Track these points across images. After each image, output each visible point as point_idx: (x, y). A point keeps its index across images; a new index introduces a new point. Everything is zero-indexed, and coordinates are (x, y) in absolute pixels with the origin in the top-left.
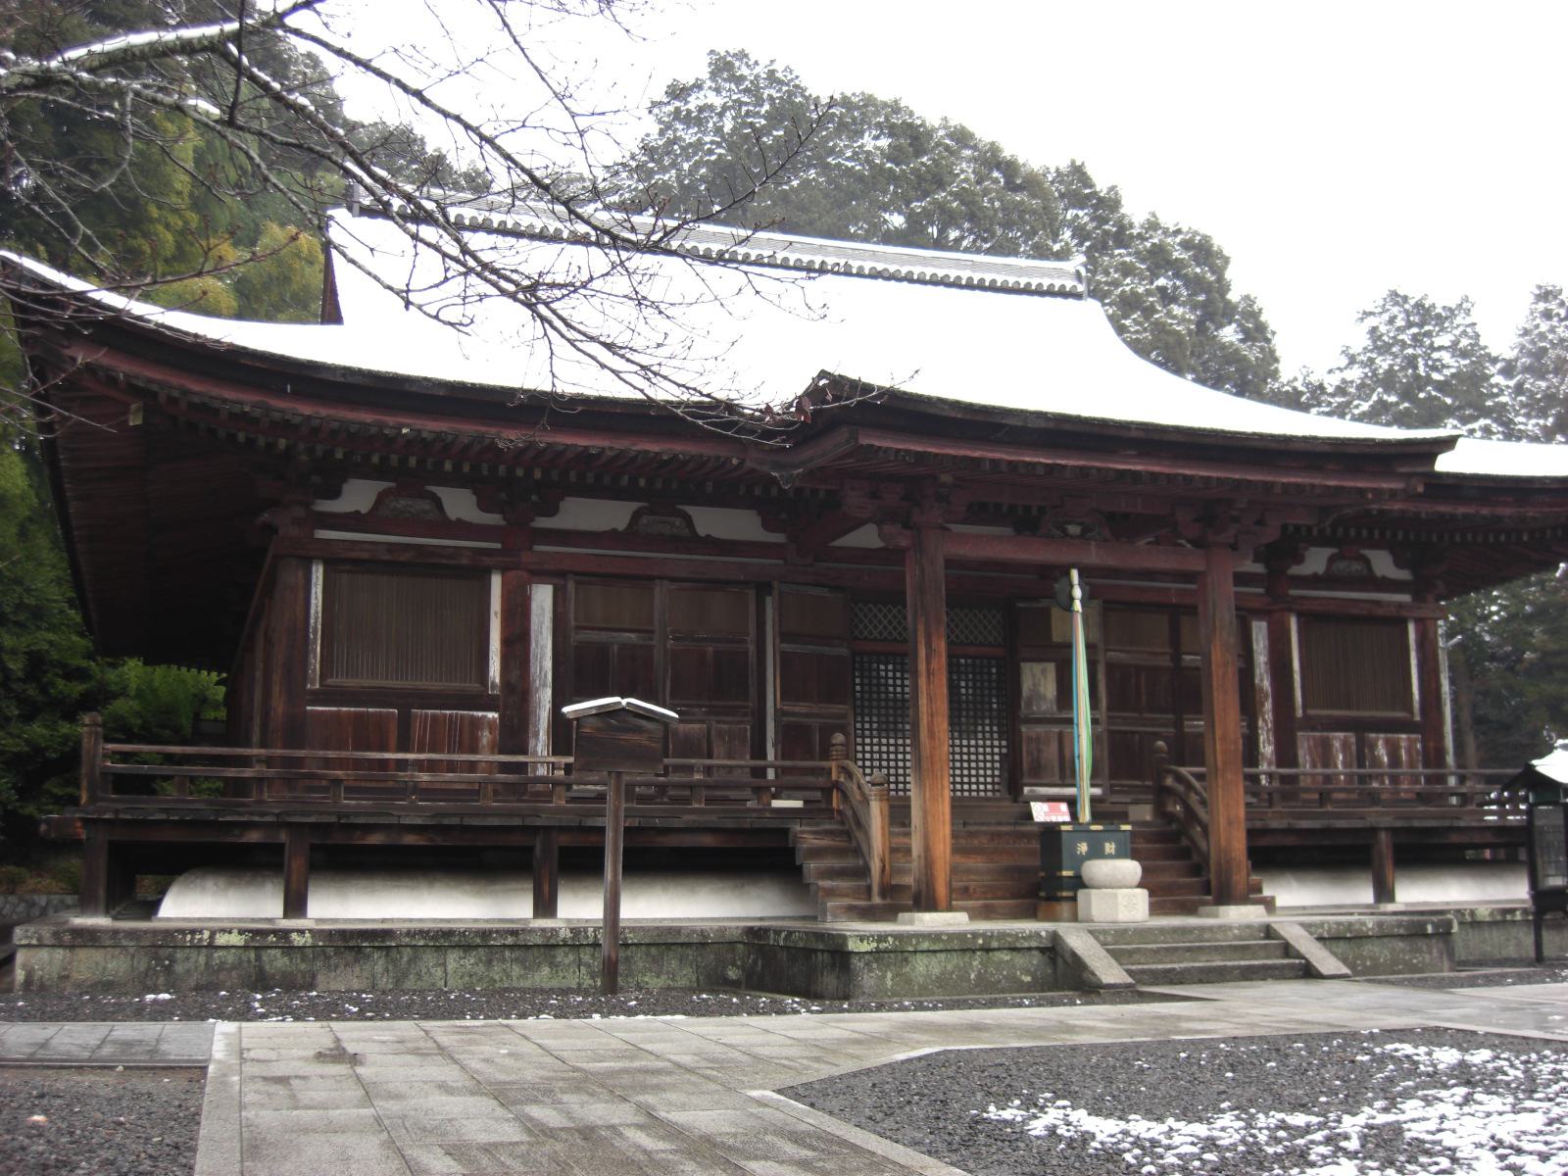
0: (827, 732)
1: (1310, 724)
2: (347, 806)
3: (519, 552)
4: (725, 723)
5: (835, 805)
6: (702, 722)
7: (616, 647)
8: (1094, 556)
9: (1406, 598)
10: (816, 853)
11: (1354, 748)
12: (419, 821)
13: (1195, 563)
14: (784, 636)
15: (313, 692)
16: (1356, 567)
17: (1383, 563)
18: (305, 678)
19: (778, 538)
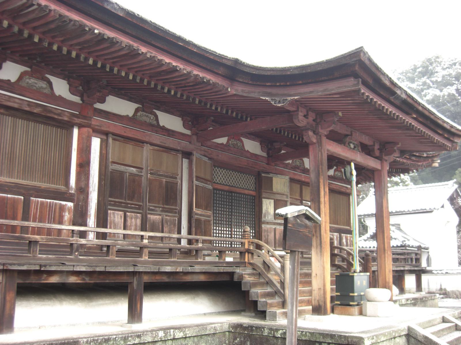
2: (41, 259)
3: (85, 116)
4: (169, 216)
5: (246, 260)
6: (160, 215)
7: (128, 174)
12: (83, 269)
16: (42, 84)
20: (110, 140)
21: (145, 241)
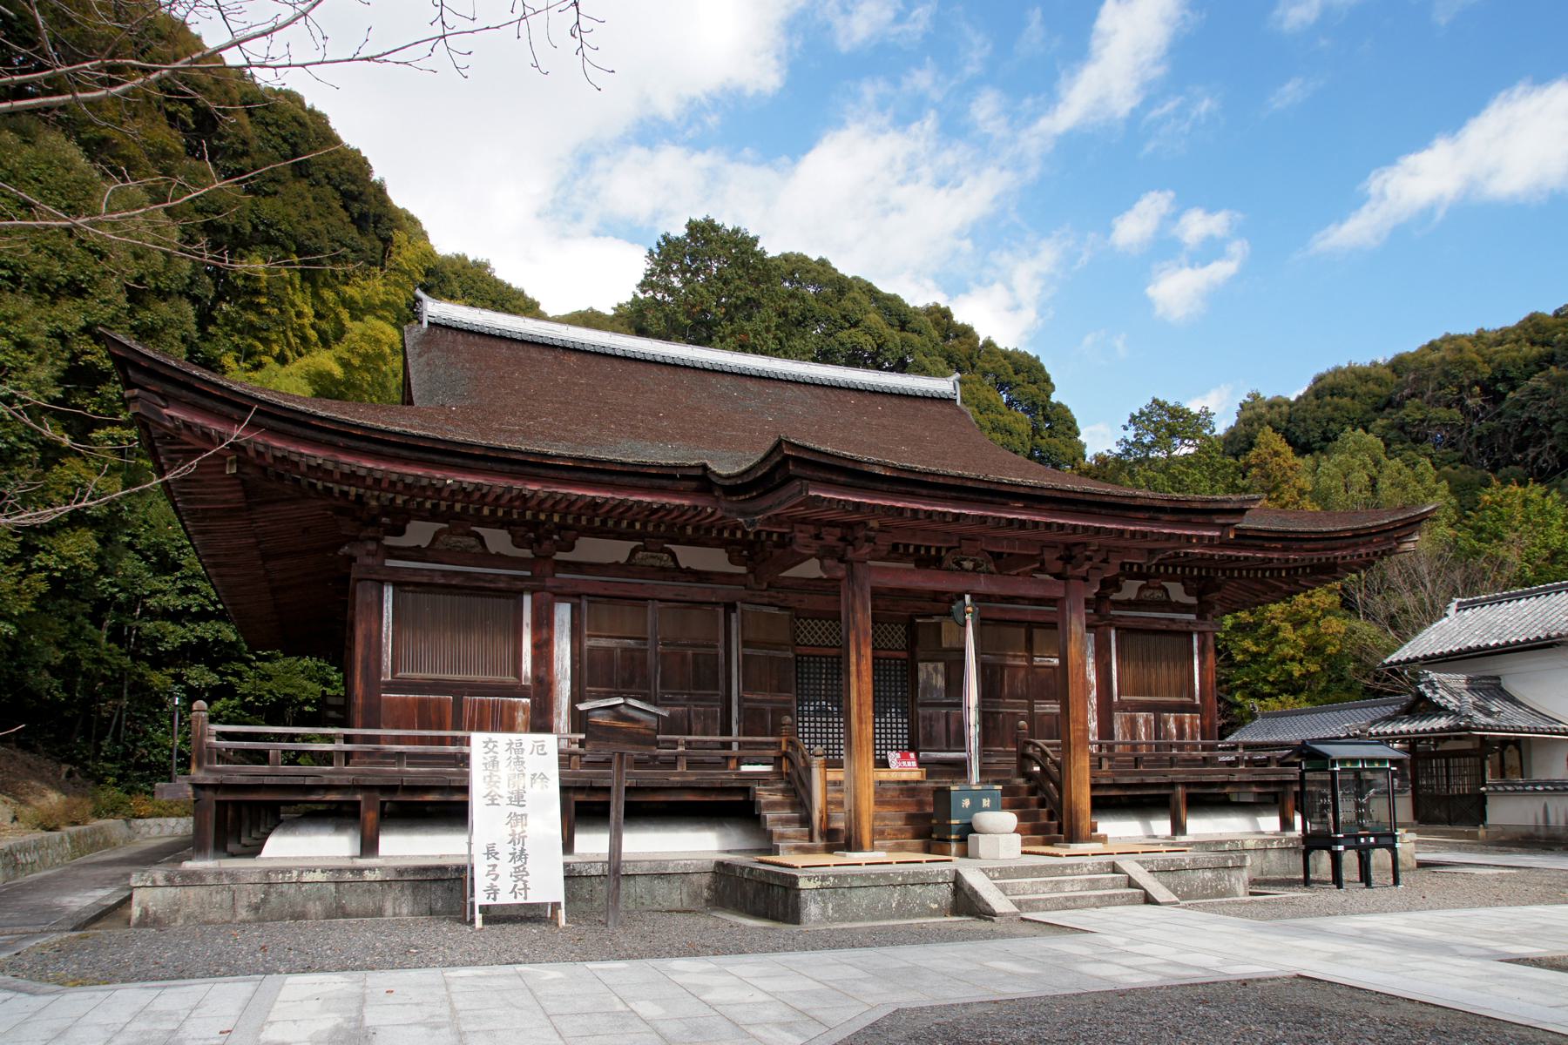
0: (778, 713)
1: (1123, 707)
8: (983, 585)
9: (1193, 617)
10: (772, 805)
13: (1058, 591)
14: (746, 643)
15: (387, 683)
16: (1159, 594)
17: (1177, 592)
18: (379, 674)
19: (742, 570)
20: (584, 604)
21: (681, 749)
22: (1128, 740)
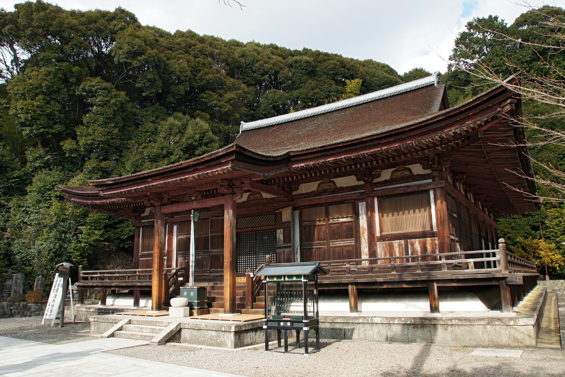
1: (383, 238)
8: (195, 205)
9: (430, 181)
11: (404, 246)
22: (388, 256)
